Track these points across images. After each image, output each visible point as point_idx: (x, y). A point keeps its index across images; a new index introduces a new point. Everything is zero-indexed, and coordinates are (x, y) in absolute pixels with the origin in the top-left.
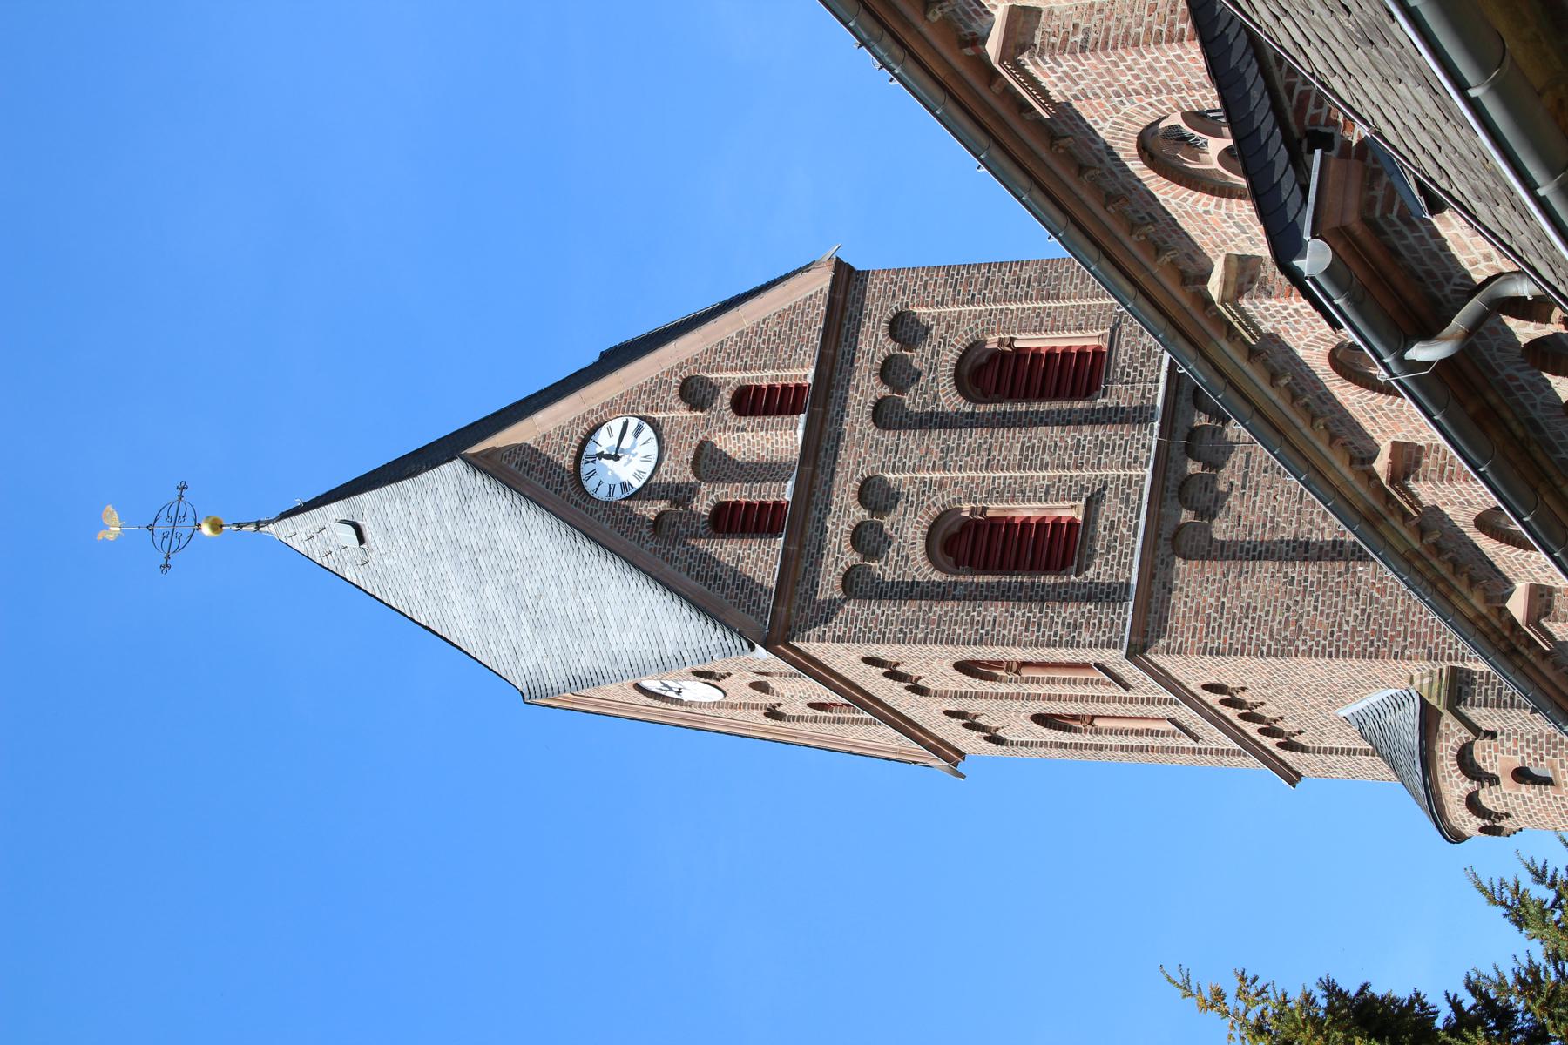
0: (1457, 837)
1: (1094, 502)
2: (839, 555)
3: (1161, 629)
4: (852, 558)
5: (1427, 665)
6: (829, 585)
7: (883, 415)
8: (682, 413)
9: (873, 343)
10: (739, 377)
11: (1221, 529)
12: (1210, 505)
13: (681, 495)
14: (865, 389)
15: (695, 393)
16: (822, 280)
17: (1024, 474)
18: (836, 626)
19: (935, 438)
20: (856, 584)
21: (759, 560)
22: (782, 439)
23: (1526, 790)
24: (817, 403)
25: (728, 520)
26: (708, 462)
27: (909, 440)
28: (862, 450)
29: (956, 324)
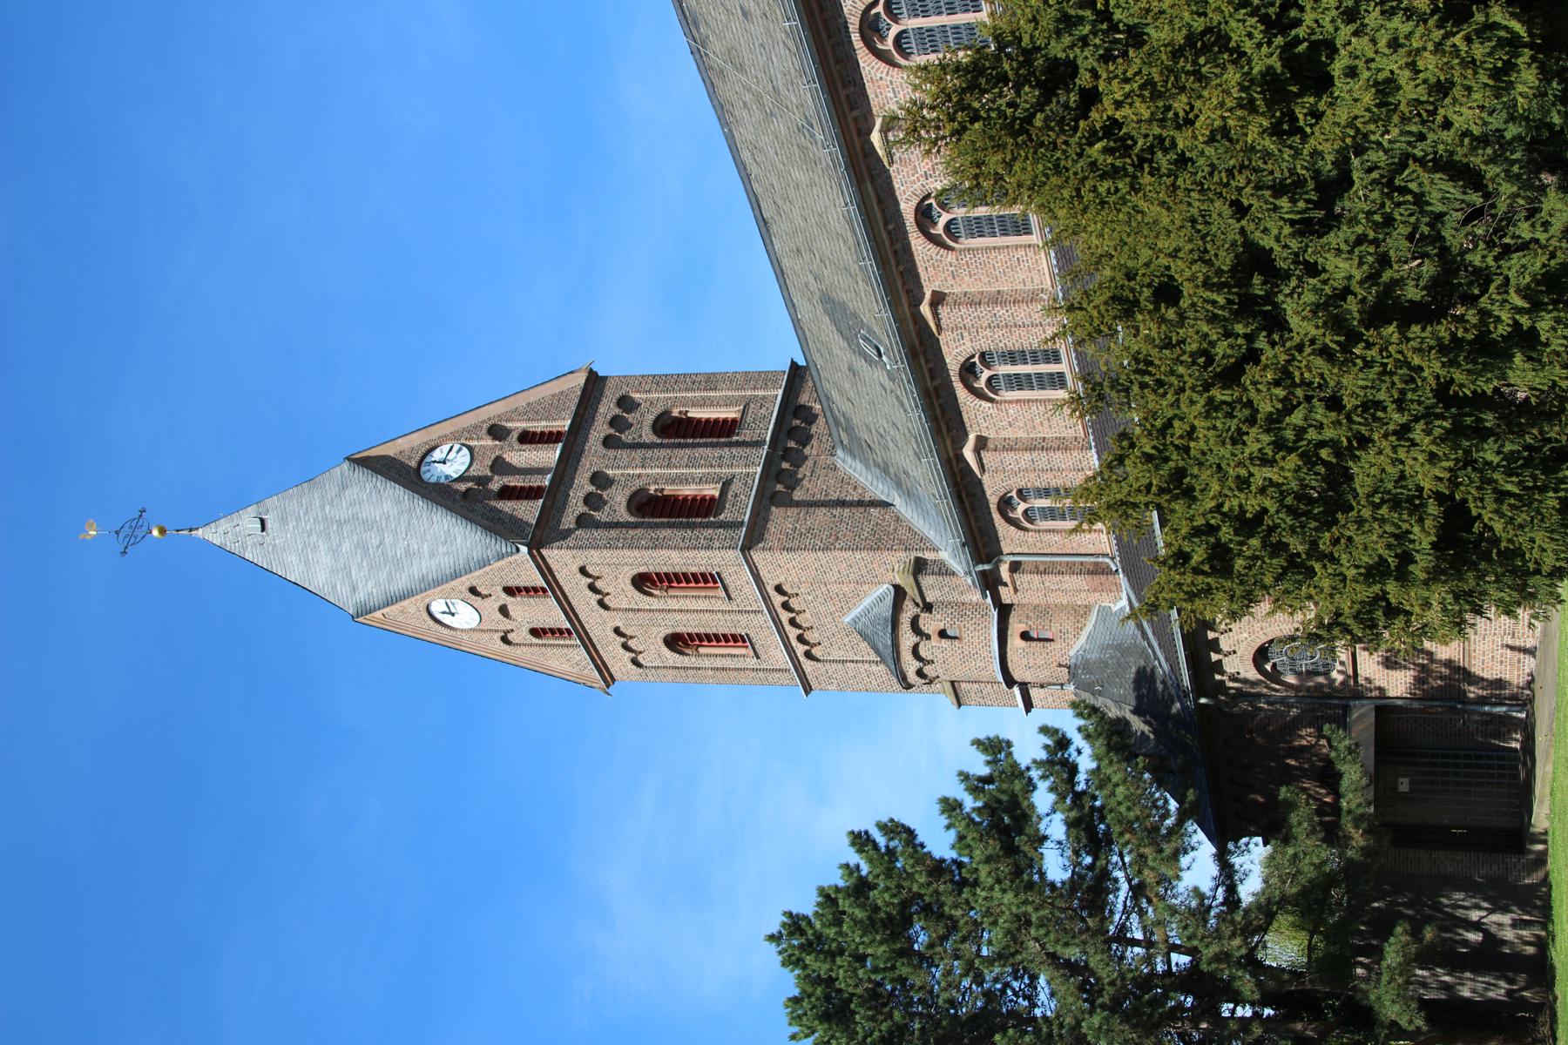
0: (908, 687)
1: (726, 485)
2: (575, 506)
3: (761, 538)
4: (582, 509)
5: (902, 555)
6: (568, 521)
7: (608, 442)
8: (489, 442)
9: (607, 408)
10: (523, 425)
11: (798, 495)
12: (793, 482)
13: (482, 481)
14: (600, 429)
15: (496, 432)
16: (580, 379)
17: (688, 474)
18: (570, 541)
19: (639, 454)
20: (583, 521)
21: (529, 511)
22: (550, 455)
23: (945, 643)
24: (572, 442)
25: (507, 493)
26: (499, 466)
27: (623, 454)
28: (594, 457)
29: (653, 402)
